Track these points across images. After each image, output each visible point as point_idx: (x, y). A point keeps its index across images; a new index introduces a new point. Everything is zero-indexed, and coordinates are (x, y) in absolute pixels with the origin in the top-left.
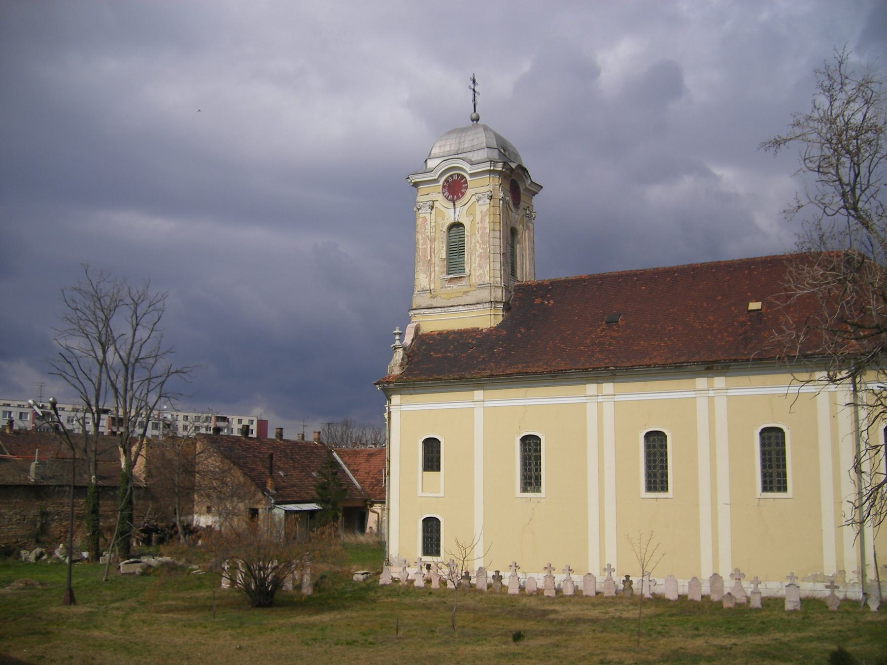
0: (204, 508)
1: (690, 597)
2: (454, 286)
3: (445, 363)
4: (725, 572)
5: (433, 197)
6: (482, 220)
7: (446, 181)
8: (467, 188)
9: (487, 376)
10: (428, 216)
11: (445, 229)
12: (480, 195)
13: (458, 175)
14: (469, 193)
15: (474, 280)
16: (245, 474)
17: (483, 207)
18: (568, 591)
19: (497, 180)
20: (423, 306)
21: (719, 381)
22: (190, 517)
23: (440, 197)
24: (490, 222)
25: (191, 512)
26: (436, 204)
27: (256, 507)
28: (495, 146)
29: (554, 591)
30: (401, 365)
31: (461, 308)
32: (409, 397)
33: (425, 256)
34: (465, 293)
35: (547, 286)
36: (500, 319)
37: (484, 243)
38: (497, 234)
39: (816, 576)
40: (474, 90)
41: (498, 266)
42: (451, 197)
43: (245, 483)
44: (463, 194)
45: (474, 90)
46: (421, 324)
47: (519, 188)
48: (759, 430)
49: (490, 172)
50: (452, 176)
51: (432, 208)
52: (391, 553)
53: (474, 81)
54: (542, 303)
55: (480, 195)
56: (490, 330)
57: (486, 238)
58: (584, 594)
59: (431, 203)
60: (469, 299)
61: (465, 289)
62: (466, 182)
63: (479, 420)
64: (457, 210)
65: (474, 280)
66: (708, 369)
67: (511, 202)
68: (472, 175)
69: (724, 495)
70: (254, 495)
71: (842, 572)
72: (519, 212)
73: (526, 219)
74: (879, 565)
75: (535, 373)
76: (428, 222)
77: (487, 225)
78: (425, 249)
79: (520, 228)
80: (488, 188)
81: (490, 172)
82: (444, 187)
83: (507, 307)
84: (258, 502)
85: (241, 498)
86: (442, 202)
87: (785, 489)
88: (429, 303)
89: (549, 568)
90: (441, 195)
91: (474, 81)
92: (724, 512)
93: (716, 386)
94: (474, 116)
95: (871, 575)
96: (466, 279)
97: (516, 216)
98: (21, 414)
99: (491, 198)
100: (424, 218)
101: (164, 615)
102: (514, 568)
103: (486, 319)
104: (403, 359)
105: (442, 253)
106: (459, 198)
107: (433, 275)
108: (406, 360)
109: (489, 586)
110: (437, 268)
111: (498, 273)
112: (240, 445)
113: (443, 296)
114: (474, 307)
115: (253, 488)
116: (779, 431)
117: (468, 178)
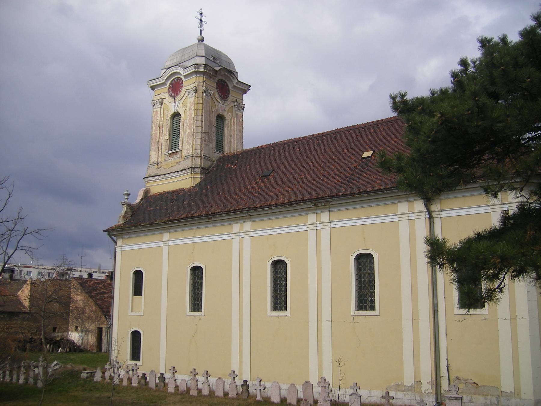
0: (74, 328)
1: (288, 401)
2: (173, 159)
3: (151, 214)
4: (314, 381)
5: (162, 96)
6: (190, 108)
7: (171, 83)
8: (183, 86)
9: (168, 221)
10: (159, 110)
11: (169, 118)
12: (190, 91)
13: (178, 78)
14: (183, 90)
15: (184, 153)
16: (96, 304)
17: (191, 99)
18: (206, 392)
19: (201, 78)
20: (152, 175)
21: (325, 216)
22: (65, 334)
23: (167, 96)
24: (194, 110)
25: (68, 330)
26: (165, 101)
27: (101, 326)
28: (204, 55)
29: (196, 391)
30: (124, 217)
31: (174, 174)
32: (126, 241)
33: (156, 139)
34: (178, 163)
35: (239, 155)
36: (198, 180)
37: (190, 126)
38: (200, 118)
39: (398, 385)
40: (201, 20)
41: (199, 141)
42: (173, 94)
43: (96, 310)
44: (180, 91)
45: (201, 20)
46: (151, 188)
47: (228, 86)
48: (354, 257)
49: (196, 73)
50: (174, 80)
51: (162, 103)
52: (112, 358)
53: (201, 14)
54: (230, 167)
55: (190, 91)
56: (193, 188)
57: (192, 122)
58: (216, 394)
59: (160, 100)
60: (180, 168)
61: (178, 160)
62: (182, 83)
63: (164, 254)
64: (177, 103)
65: (184, 153)
66: (315, 205)
67: (217, 95)
68: (186, 76)
69: (327, 314)
70: (101, 318)
71: (419, 383)
72: (227, 103)
73: (235, 109)
74: (453, 377)
75: (198, 216)
76: (159, 115)
77: (193, 112)
78: (156, 134)
79: (228, 116)
80: (194, 85)
81: (196, 73)
82: (169, 88)
83: (205, 171)
84: (102, 323)
85: (93, 321)
86: (168, 100)
87: (373, 308)
88: (157, 172)
89: (194, 373)
90: (167, 94)
91: (201, 14)
92: (327, 327)
93: (322, 220)
94: (200, 38)
95: (445, 386)
96: (179, 153)
97: (222, 107)
98: (28, 271)
99: (196, 91)
100: (157, 111)
101: (451, 396)
102: (172, 371)
103: (186, 181)
104: (126, 212)
105: (166, 136)
106: (178, 94)
107: (160, 152)
108: (130, 213)
109: (157, 385)
110: (163, 147)
111: (199, 147)
112: (104, 285)
113: (165, 167)
114: (181, 173)
115: (100, 314)
116: (369, 256)
117: (184, 79)
